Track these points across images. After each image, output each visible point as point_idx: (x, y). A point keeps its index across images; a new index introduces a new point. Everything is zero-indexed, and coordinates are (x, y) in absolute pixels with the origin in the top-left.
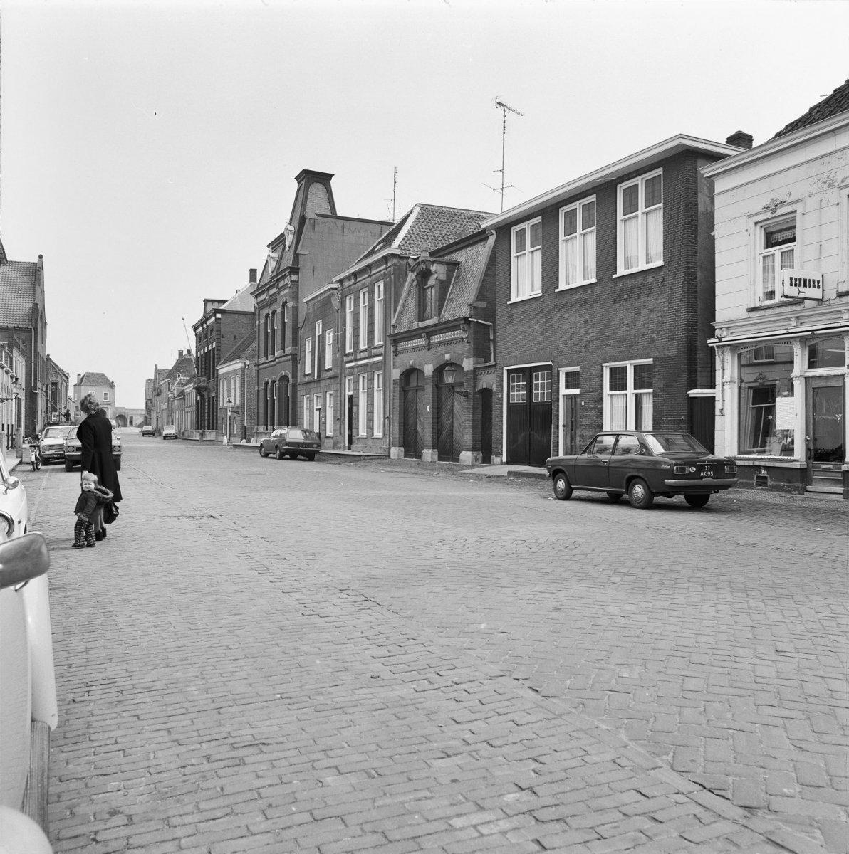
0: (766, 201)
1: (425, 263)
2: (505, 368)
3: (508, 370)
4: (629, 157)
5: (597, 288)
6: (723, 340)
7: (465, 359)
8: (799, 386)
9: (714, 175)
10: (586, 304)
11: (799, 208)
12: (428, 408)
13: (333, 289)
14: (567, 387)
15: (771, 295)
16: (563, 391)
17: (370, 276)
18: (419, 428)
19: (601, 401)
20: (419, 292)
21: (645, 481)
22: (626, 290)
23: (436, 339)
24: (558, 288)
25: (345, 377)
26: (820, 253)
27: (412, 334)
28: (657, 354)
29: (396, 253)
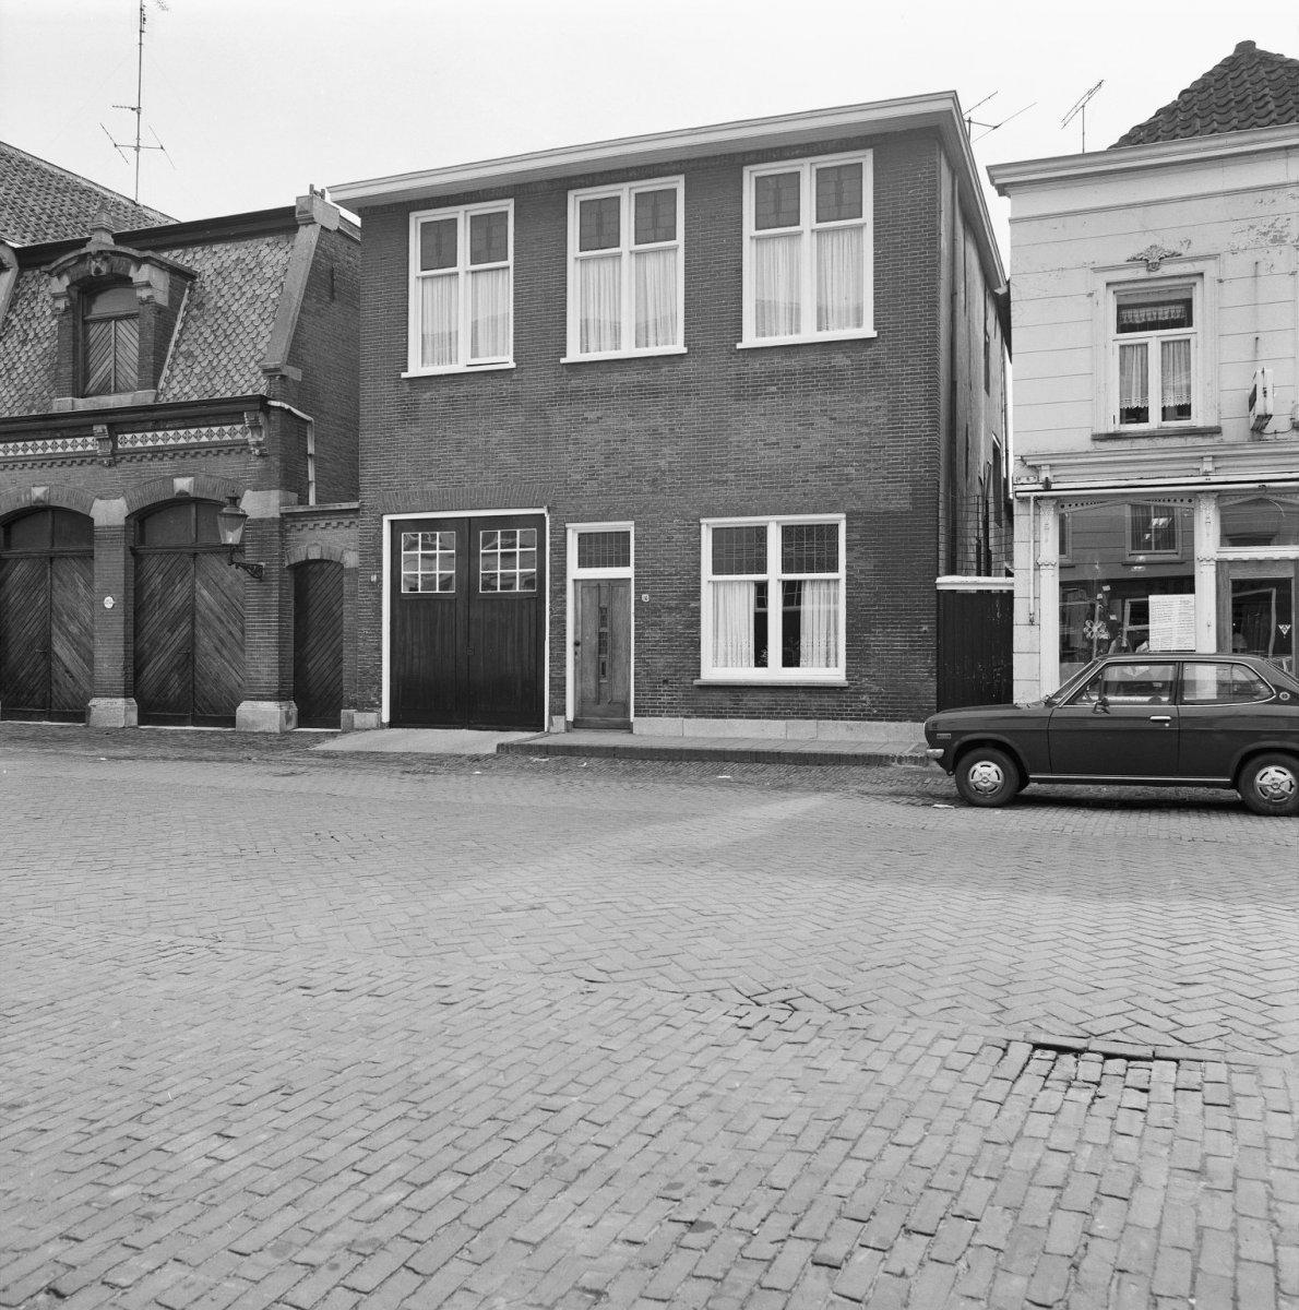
0: (1139, 247)
1: (106, 259)
2: (386, 518)
4: (813, 114)
5: (690, 366)
6: (1054, 486)
7: (248, 493)
8: (1206, 578)
9: (1012, 184)
10: (656, 394)
11: (1209, 268)
12: (109, 602)
14: (582, 563)
15: (1138, 415)
16: (575, 572)
18: (61, 648)
19: (695, 594)
20: (75, 327)
22: (772, 377)
23: (128, 441)
24: (565, 356)
26: (1257, 351)
27: (52, 423)
28: (858, 506)
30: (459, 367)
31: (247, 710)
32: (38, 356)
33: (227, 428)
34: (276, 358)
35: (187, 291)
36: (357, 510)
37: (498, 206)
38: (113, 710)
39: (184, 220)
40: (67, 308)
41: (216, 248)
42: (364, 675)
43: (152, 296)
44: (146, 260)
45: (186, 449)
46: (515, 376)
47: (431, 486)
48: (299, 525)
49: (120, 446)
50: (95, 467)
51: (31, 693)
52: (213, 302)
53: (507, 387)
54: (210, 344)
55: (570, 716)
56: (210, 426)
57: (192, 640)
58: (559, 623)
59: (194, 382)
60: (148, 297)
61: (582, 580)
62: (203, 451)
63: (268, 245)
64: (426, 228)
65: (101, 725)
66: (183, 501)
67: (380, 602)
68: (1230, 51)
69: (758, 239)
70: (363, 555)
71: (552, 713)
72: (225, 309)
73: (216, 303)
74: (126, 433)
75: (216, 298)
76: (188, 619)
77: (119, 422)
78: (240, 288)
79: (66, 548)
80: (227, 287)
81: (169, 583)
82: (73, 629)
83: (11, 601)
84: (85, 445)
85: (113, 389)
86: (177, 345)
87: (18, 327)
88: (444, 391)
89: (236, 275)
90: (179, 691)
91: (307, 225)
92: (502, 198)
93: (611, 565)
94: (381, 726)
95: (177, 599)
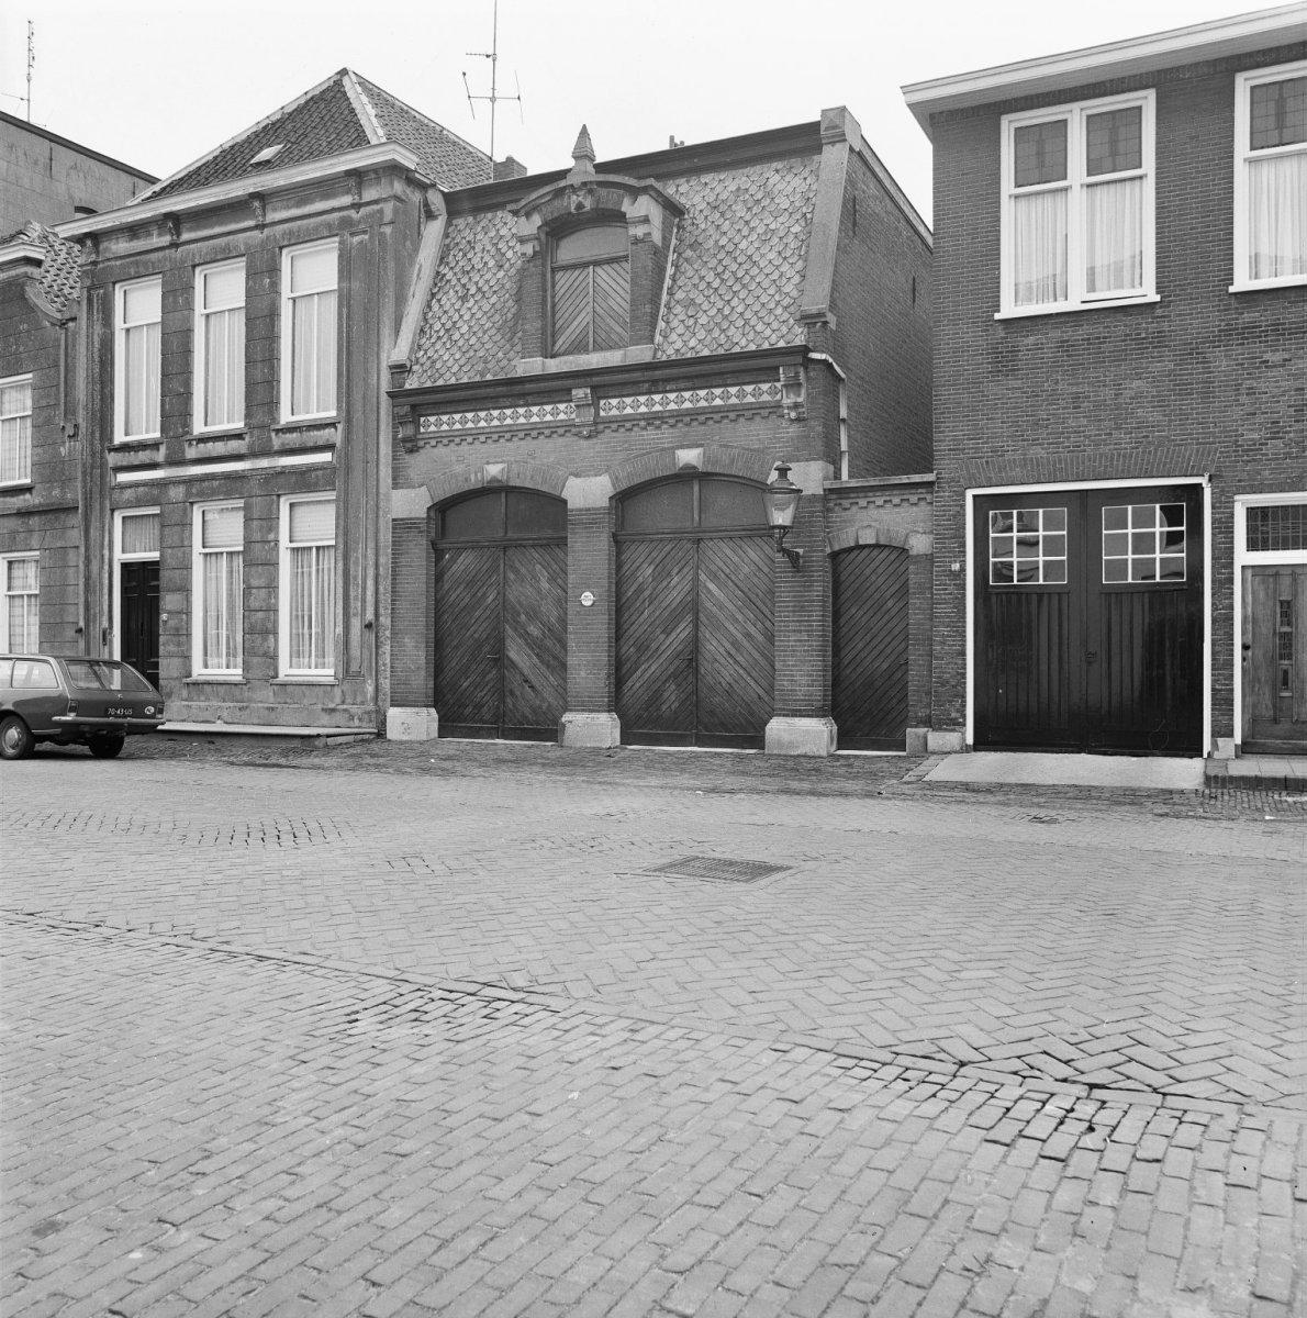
1: (590, 192)
2: (970, 494)
3: (975, 497)
12: (587, 599)
13: (28, 261)
14: (1253, 545)
16: (1243, 556)
17: (261, 227)
18: (517, 653)
21: (22, 719)
23: (612, 407)
25: (113, 511)
27: (518, 389)
29: (407, 163)
30: (1073, 304)
31: (779, 729)
32: (486, 313)
33: (749, 388)
34: (817, 301)
35: (675, 230)
36: (931, 484)
37: (1128, 100)
38: (594, 727)
39: (688, 143)
40: (535, 253)
41: (705, 178)
42: (943, 685)
43: (649, 234)
44: (645, 190)
45: (693, 414)
46: (1159, 312)
47: (1038, 452)
48: (846, 503)
49: (602, 413)
50: (569, 439)
51: (479, 706)
52: (711, 242)
53: (1146, 325)
54: (716, 289)
55: (1238, 739)
56: (542, 404)
57: (695, 644)
58: (1224, 621)
59: (701, 334)
60: (645, 234)
61: (1253, 567)
62: (717, 417)
63: (777, 171)
64: (1020, 133)
65: (578, 745)
66: (688, 476)
67: (964, 595)
68: (810, 115)
69: (1250, 161)
70: (939, 538)
71: (1215, 734)
72: (730, 247)
73: (717, 242)
74: (716, 387)
75: (716, 236)
76: (689, 618)
77: (604, 383)
78: (747, 223)
79: (527, 536)
80: (727, 222)
81: (662, 574)
82: (534, 630)
83: (452, 598)
84: (555, 413)
85: (591, 346)
86: (671, 294)
87: (454, 282)
88: (1056, 334)
89: (740, 210)
90: (677, 704)
91: (833, 143)
92: (1136, 89)
93: (1285, 548)
94: (966, 749)
95: (676, 590)
